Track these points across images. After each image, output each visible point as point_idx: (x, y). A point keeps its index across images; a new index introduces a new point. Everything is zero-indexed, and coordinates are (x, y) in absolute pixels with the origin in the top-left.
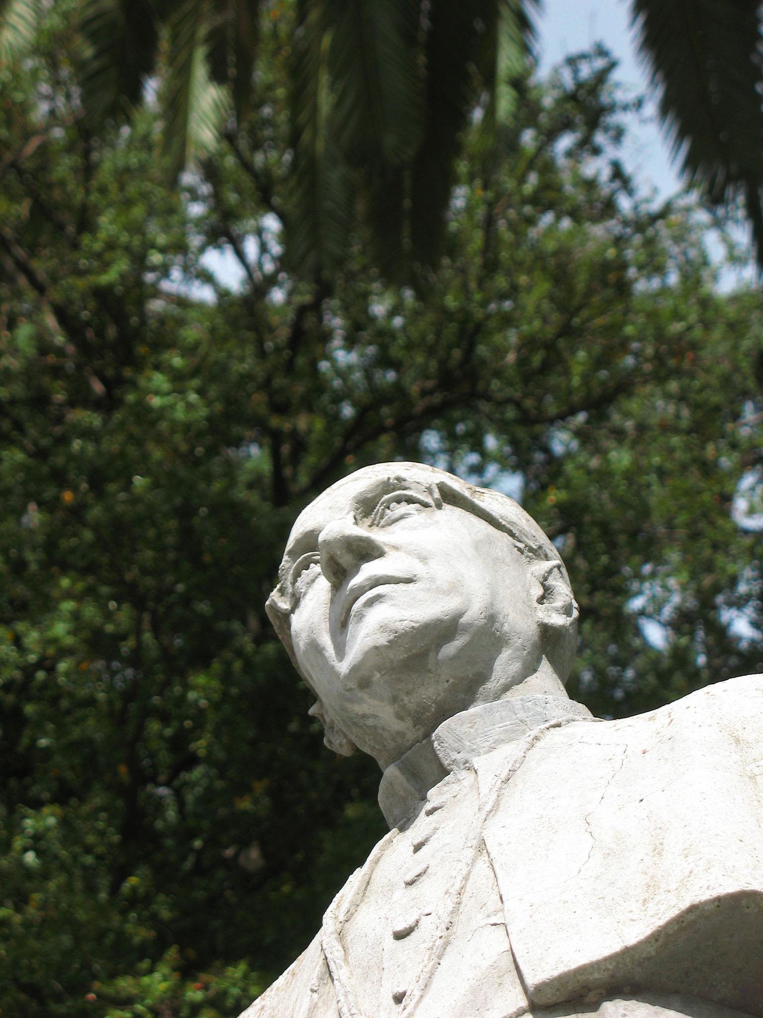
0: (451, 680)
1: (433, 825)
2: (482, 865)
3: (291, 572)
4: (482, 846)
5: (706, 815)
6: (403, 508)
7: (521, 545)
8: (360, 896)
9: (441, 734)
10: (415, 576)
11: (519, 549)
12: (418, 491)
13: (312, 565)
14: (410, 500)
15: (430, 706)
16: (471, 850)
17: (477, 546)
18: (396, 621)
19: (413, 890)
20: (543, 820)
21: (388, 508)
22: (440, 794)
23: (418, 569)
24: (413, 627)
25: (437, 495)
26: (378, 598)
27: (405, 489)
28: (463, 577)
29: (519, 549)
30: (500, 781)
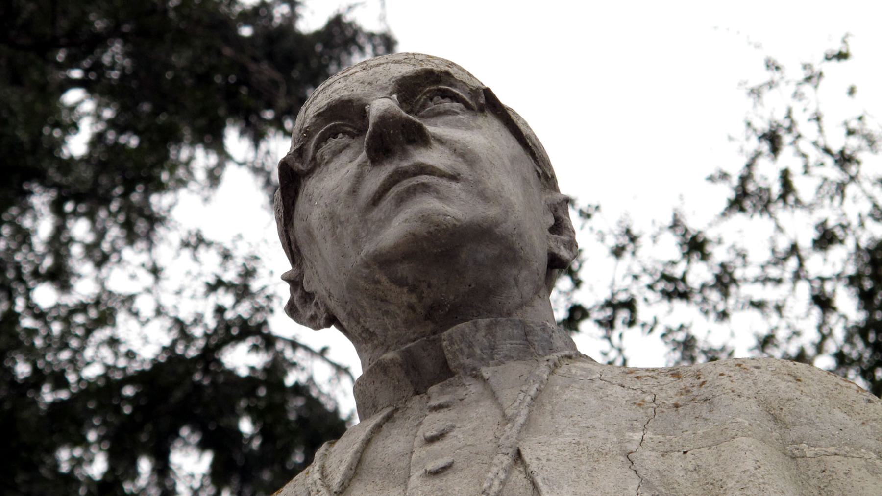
0: (473, 286)
1: (449, 423)
2: (518, 476)
3: (317, 136)
4: (518, 456)
5: (764, 483)
6: (447, 104)
7: (540, 171)
8: (352, 472)
9: (454, 335)
10: (459, 175)
11: (538, 173)
12: (463, 90)
13: (340, 135)
14: (455, 98)
15: (446, 305)
16: (507, 457)
17: (513, 160)
18: (439, 215)
19: (437, 482)
20: (581, 446)
21: (431, 100)
22: (442, 392)
23: (463, 168)
24: (455, 225)
25: (482, 101)
26: (425, 188)
27: (451, 85)
28: (503, 188)
29: (538, 173)
30: (528, 398)
